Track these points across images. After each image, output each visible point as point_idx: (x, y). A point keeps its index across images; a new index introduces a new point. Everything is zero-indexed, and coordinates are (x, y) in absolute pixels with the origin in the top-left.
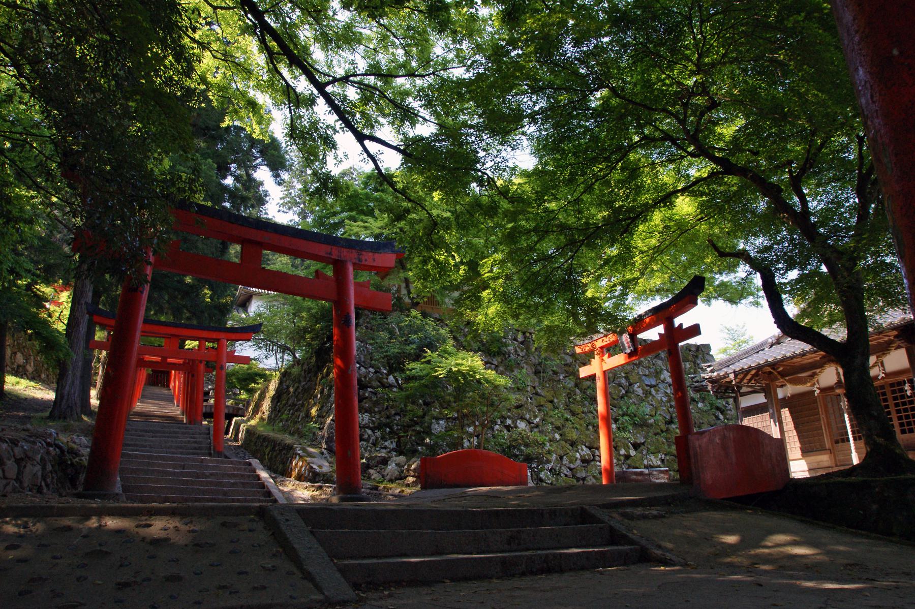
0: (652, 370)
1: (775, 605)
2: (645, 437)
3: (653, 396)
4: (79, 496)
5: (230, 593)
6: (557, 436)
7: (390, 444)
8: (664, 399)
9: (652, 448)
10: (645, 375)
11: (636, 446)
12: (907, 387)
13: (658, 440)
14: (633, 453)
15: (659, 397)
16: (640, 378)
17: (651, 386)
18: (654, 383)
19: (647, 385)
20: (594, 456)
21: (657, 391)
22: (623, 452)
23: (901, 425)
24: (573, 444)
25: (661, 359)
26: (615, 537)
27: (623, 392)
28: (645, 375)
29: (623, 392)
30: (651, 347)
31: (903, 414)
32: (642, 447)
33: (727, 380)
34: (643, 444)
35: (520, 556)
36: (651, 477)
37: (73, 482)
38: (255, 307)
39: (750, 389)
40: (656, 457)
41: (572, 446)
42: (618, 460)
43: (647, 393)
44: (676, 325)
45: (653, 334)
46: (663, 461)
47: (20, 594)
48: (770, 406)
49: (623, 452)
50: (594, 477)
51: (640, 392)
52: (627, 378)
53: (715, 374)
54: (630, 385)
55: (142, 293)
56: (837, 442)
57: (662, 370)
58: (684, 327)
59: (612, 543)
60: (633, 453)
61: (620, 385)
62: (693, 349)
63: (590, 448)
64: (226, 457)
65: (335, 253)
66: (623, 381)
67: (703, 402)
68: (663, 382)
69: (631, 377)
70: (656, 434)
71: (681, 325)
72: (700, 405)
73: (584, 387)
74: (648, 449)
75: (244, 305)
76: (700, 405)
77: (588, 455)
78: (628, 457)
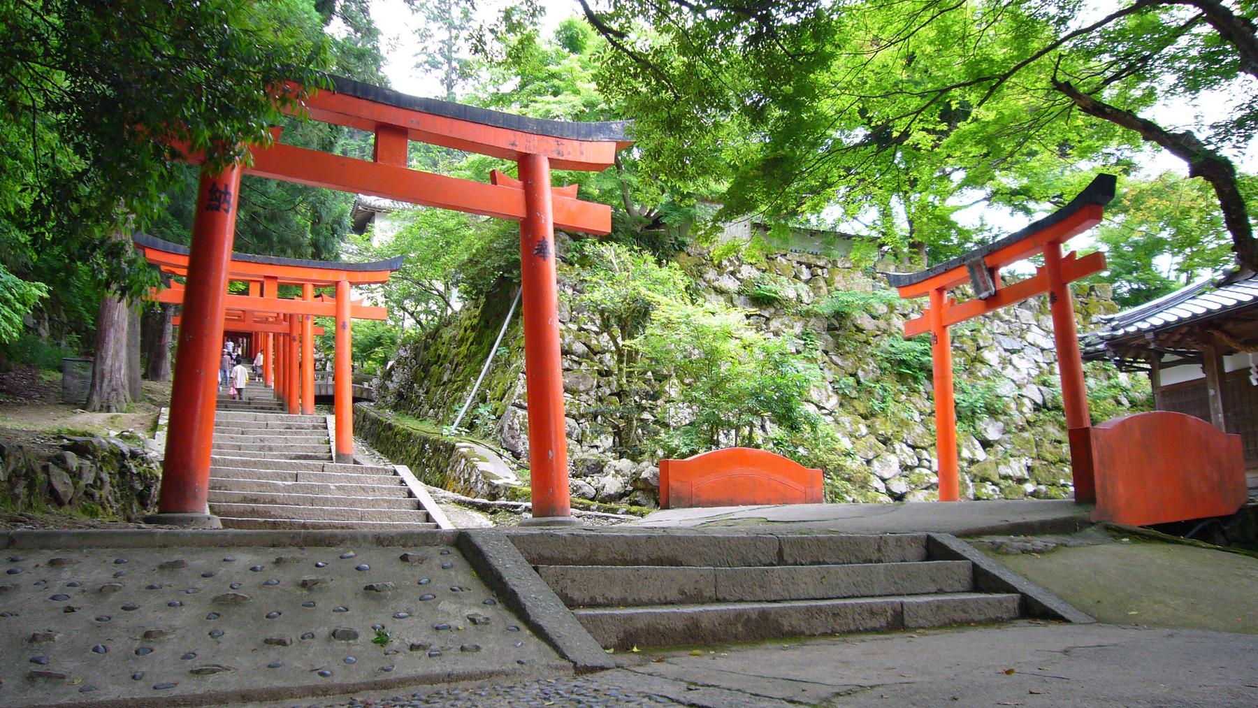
1: (151, 587)
4: (148, 520)
5: (430, 655)
6: (864, 430)
7: (607, 441)
17: (1013, 352)
18: (1017, 347)
19: (1006, 350)
20: (920, 460)
24: (886, 441)
26: (982, 581)
30: (1020, 292)
33: (1140, 342)
35: (846, 606)
37: (143, 499)
38: (384, 233)
39: (1177, 358)
41: (884, 443)
43: (1006, 362)
44: (1064, 253)
45: (1025, 268)
47: (137, 652)
48: (1210, 384)
55: (227, 211)
58: (1078, 256)
59: (976, 588)
64: (355, 462)
65: (524, 143)
71: (1073, 254)
75: (362, 223)
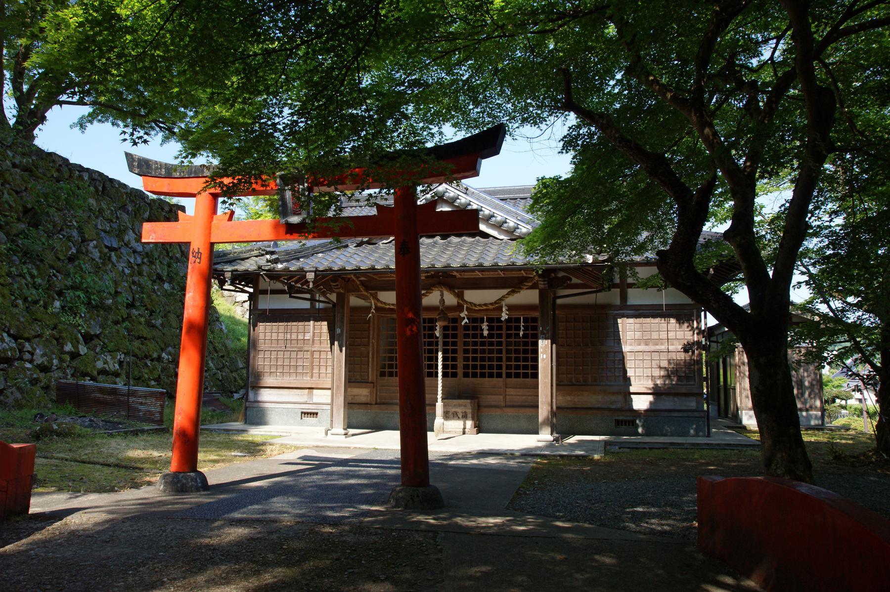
0: (115, 226)
2: (102, 327)
3: (114, 265)
8: (127, 271)
9: (111, 346)
10: (105, 231)
11: (88, 338)
12: (485, 326)
13: (118, 331)
14: (83, 349)
15: (121, 266)
16: (98, 234)
17: (111, 249)
18: (115, 245)
19: (107, 247)
20: (21, 351)
21: (119, 257)
22: (68, 347)
23: (466, 367)
25: (128, 213)
27: (74, 250)
28: (105, 231)
29: (74, 250)
31: (487, 363)
32: (96, 341)
34: (97, 336)
36: (131, 399)
40: (113, 358)
42: (61, 360)
46: (121, 363)
49: (68, 347)
50: (19, 389)
51: (96, 254)
52: (80, 230)
53: (280, 266)
54: (83, 241)
56: (382, 374)
57: (127, 228)
60: (83, 349)
61: (69, 238)
62: (167, 209)
63: (15, 338)
66: (75, 233)
67: (170, 283)
68: (126, 245)
69: (86, 230)
70: (116, 323)
72: (166, 286)
73: (14, 232)
74: (104, 346)
76: (166, 286)
77: (11, 349)
78: (75, 355)
